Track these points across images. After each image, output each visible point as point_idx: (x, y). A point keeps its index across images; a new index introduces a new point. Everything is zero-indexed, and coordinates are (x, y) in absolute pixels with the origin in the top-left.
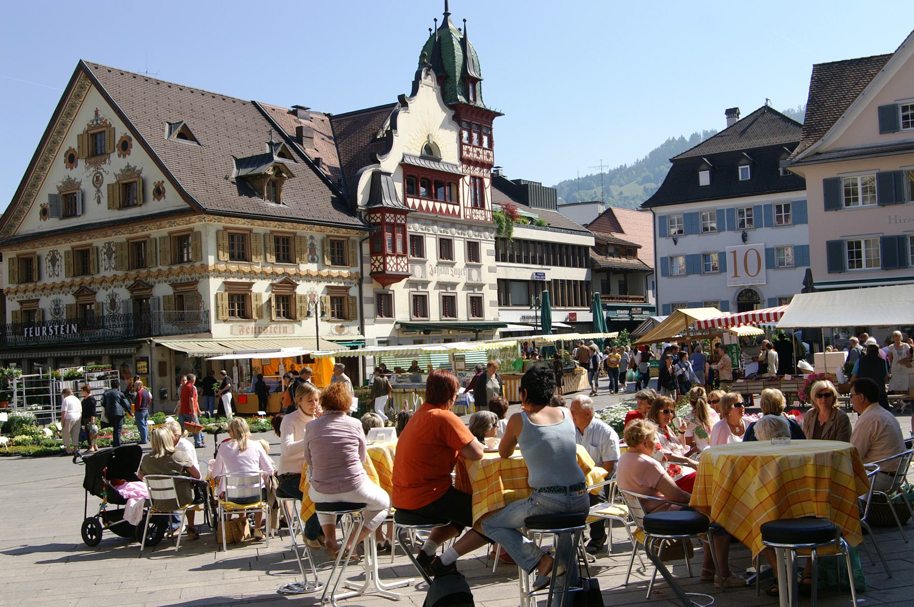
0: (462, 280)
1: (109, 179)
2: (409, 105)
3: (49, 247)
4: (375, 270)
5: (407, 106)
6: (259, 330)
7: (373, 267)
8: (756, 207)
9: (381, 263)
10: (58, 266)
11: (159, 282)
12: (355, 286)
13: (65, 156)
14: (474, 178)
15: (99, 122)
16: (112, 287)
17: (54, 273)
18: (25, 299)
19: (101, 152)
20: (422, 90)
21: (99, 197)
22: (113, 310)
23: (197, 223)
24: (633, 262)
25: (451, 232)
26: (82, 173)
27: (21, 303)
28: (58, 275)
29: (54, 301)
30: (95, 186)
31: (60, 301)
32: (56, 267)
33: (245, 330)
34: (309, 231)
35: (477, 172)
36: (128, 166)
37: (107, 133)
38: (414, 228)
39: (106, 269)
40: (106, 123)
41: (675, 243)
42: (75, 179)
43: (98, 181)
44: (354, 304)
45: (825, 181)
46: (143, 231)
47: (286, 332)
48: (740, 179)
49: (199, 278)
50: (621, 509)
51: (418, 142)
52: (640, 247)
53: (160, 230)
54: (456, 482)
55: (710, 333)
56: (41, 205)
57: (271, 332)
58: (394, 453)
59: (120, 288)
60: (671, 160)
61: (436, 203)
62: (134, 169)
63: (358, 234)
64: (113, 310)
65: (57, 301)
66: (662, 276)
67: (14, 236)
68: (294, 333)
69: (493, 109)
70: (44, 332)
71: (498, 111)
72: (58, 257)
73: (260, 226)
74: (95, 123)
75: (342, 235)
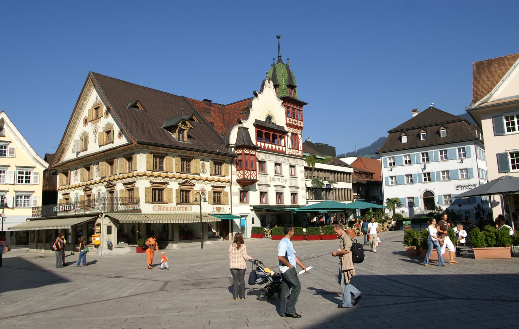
0: (287, 185)
1: (100, 130)
2: (259, 96)
4: (239, 178)
5: (258, 97)
6: (170, 209)
7: (238, 176)
9: (242, 174)
11: (119, 183)
12: (228, 186)
13: (83, 120)
14: (292, 134)
15: (98, 102)
16: (99, 186)
17: (76, 179)
20: (266, 89)
21: (95, 139)
23: (136, 150)
25: (281, 159)
26: (90, 128)
28: (77, 180)
30: (94, 134)
33: (162, 209)
34: (201, 156)
35: (295, 131)
36: (108, 123)
43: (95, 131)
44: (227, 196)
47: (187, 210)
51: (264, 115)
52: (374, 174)
53: (120, 154)
57: (178, 210)
61: (273, 146)
62: (110, 124)
63: (229, 159)
68: (191, 210)
69: (302, 101)
70: (61, 209)
71: (305, 102)
73: (172, 152)
75: (220, 159)
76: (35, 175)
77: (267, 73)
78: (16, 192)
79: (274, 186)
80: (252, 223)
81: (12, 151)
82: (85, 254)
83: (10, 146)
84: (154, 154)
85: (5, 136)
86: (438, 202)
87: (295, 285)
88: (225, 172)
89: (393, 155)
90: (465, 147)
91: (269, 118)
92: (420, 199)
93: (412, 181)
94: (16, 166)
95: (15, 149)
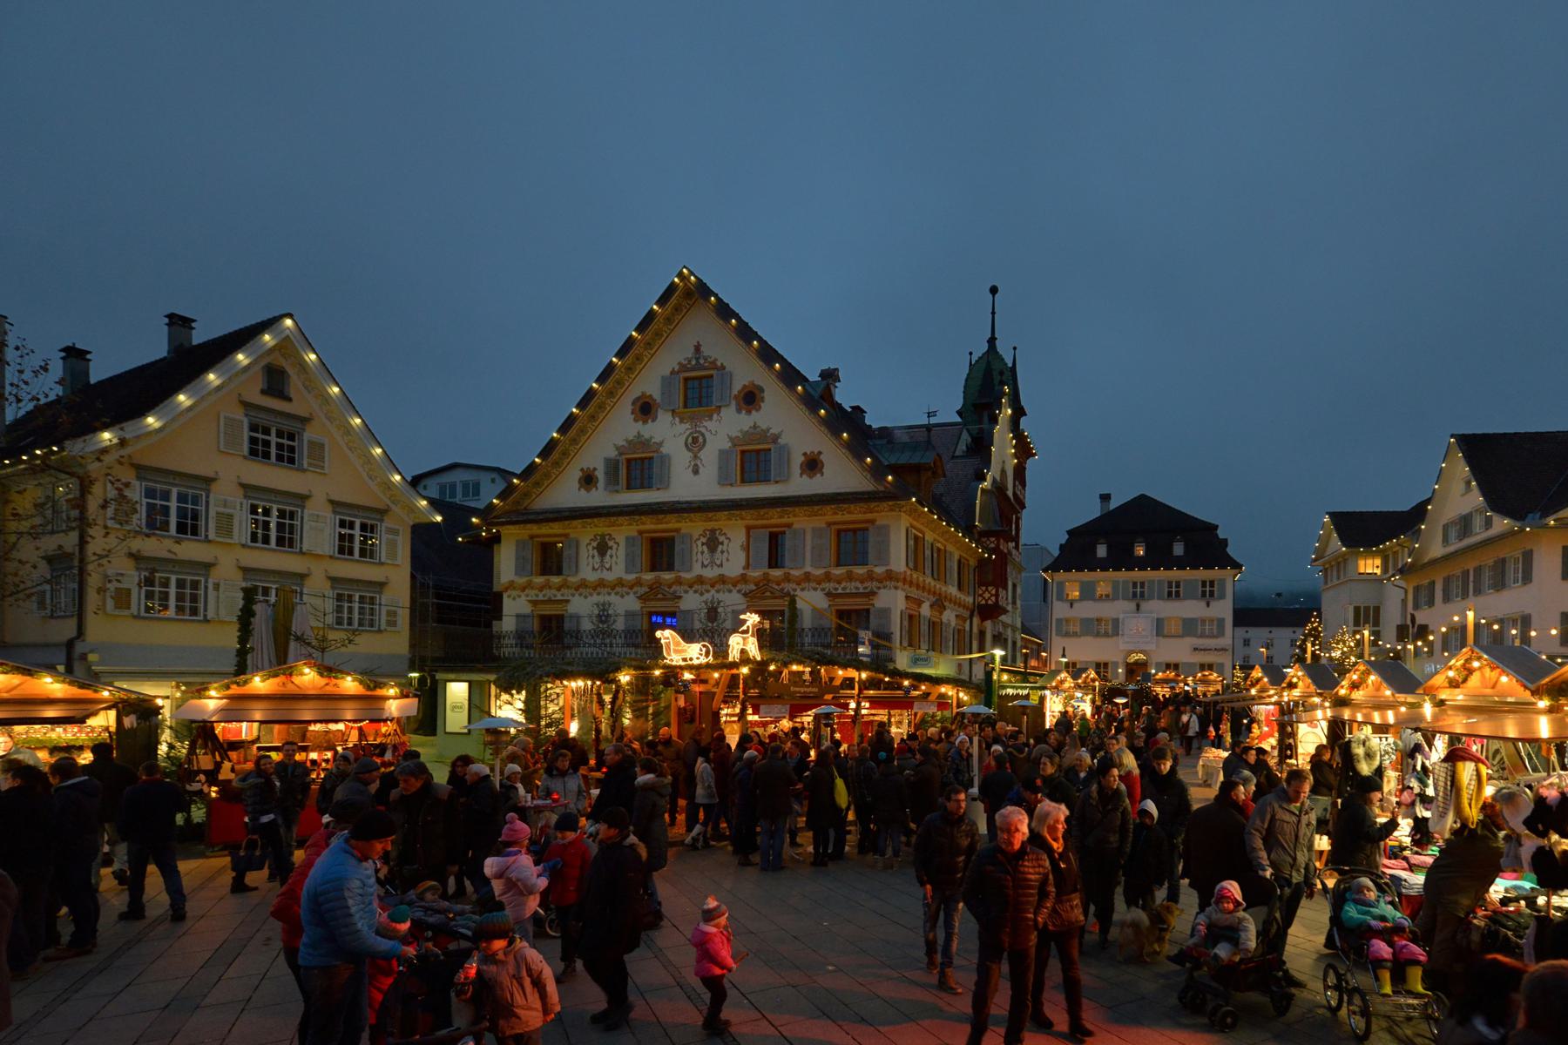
3: (596, 529)
8: (1149, 581)
10: (611, 556)
13: (633, 404)
15: (702, 361)
18: (541, 598)
21: (696, 465)
22: (713, 623)
26: (667, 432)
27: (535, 603)
28: (610, 569)
29: (598, 606)
31: (610, 604)
32: (608, 557)
37: (716, 381)
39: (703, 566)
40: (716, 365)
41: (1208, 605)
42: (651, 438)
46: (781, 517)
49: (879, 588)
50: (85, 759)
54: (698, 812)
56: (582, 470)
59: (727, 594)
64: (713, 623)
65: (603, 605)
67: (525, 509)
72: (611, 543)
74: (694, 362)
76: (391, 537)
78: (246, 570)
81: (317, 449)
83: (309, 434)
85: (290, 400)
87: (169, 694)
94: (332, 502)
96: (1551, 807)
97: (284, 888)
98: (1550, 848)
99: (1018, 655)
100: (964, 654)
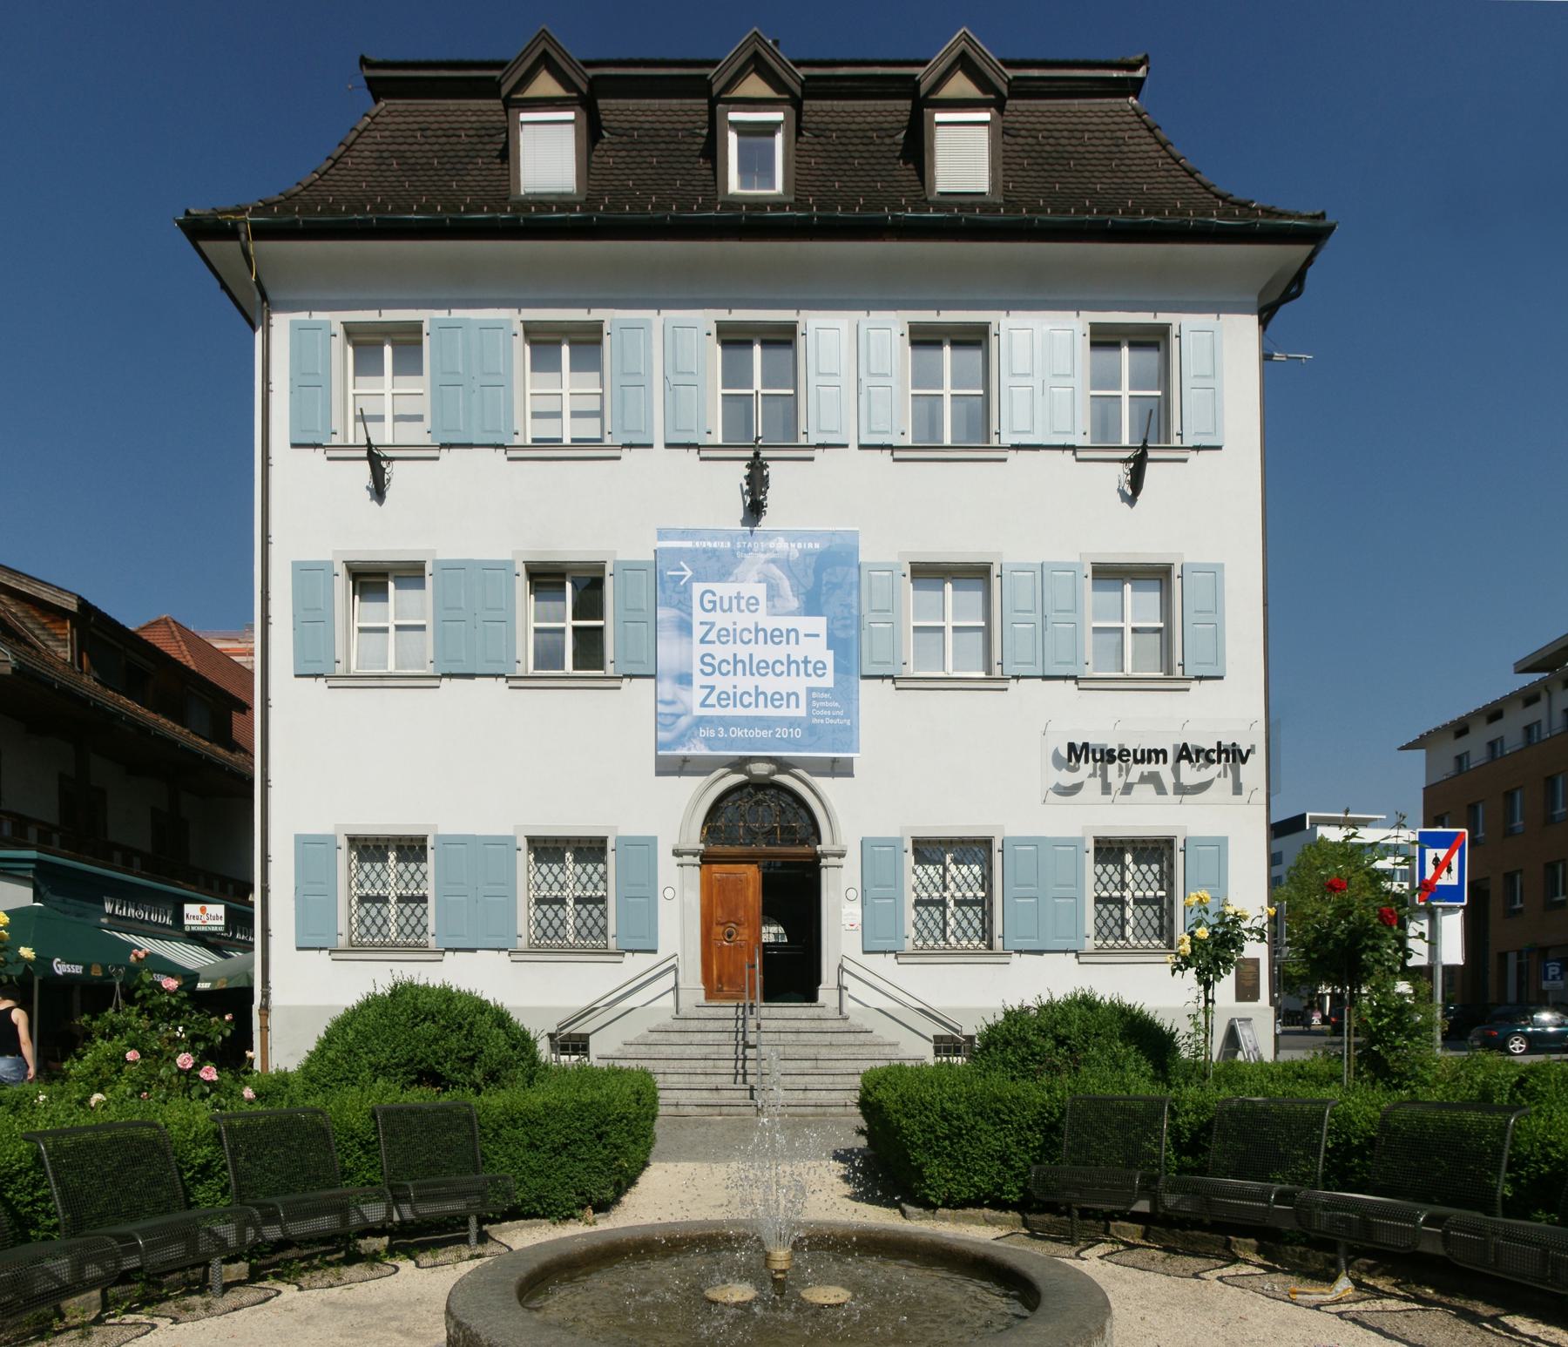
19: (593, 174)
24: (724, 315)
38: (1328, 1027)
45: (1258, 959)
48: (734, 185)
55: (1154, 1205)
58: (237, 659)
60: (8, 913)
66: (1092, 325)
77: (1085, 434)
79: (359, 76)
80: (1234, 794)
82: (211, 940)
84: (397, 338)
86: (1180, 574)
88: (824, 1097)
89: (589, 305)
90: (1425, 827)
91: (187, 213)
92: (667, 867)
93: (590, 648)
95: (813, 1004)
96: (960, 69)
97: (1499, 1199)
98: (535, 1039)
99: (714, 950)
100: (252, 915)
